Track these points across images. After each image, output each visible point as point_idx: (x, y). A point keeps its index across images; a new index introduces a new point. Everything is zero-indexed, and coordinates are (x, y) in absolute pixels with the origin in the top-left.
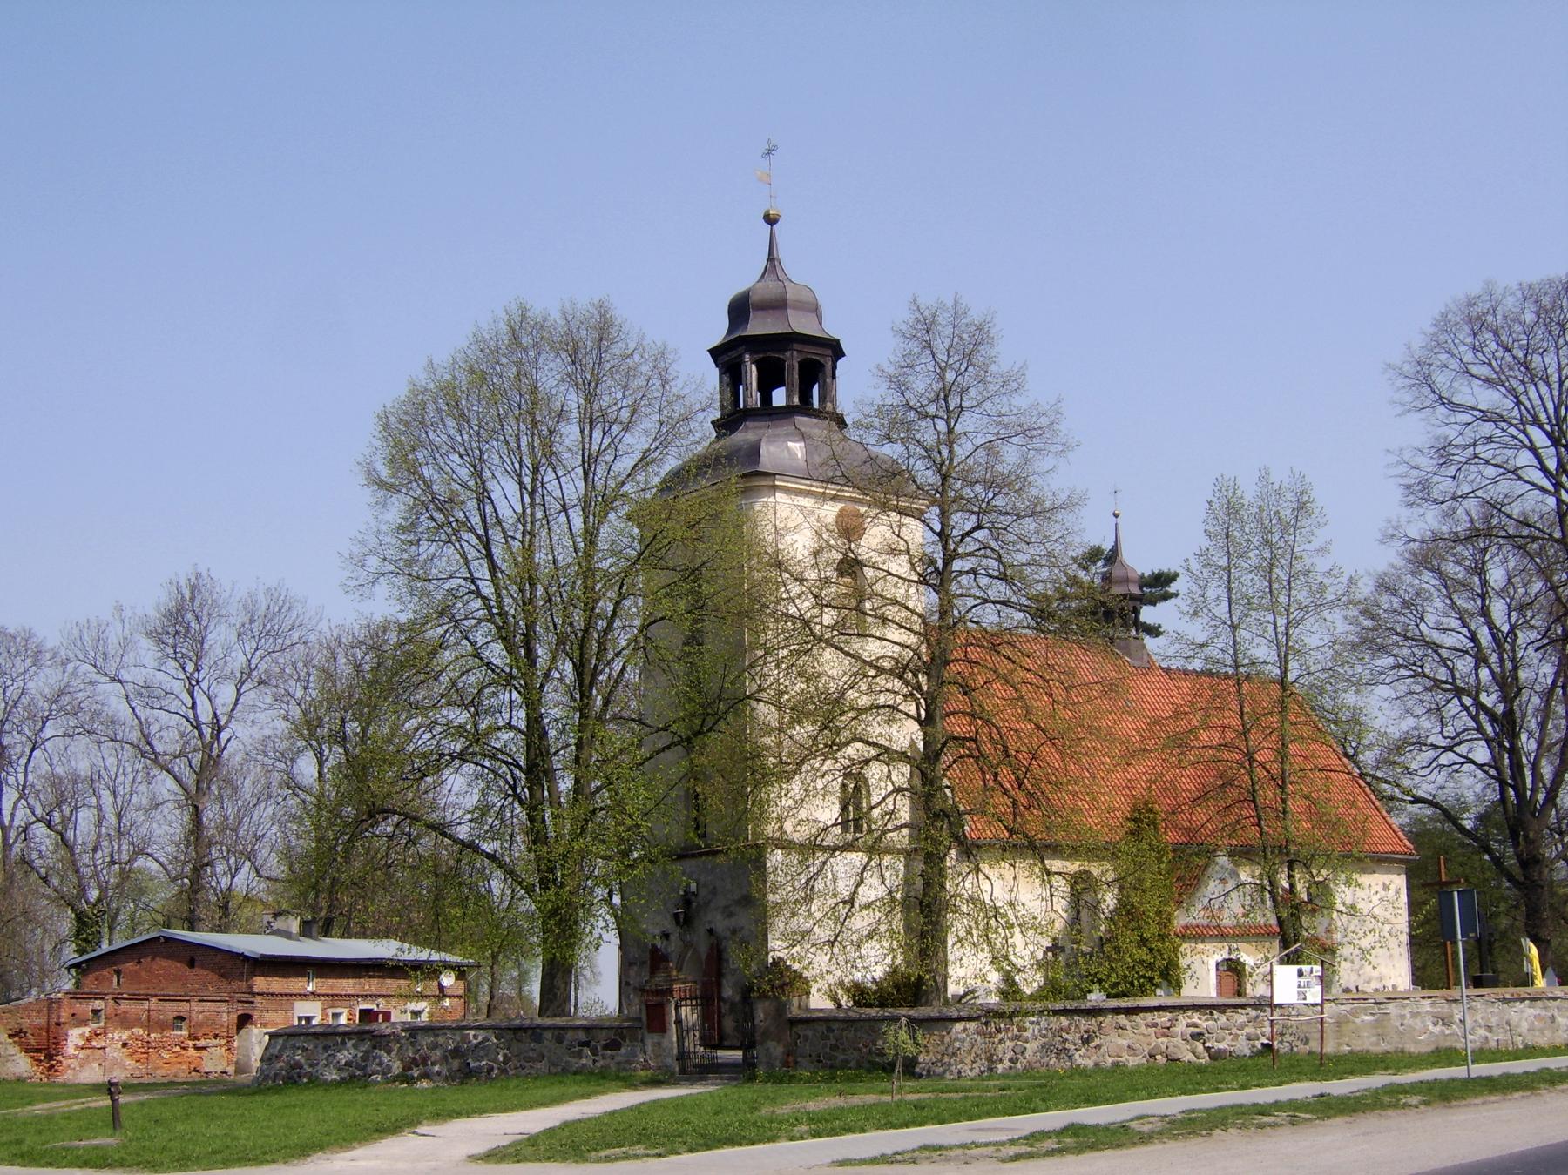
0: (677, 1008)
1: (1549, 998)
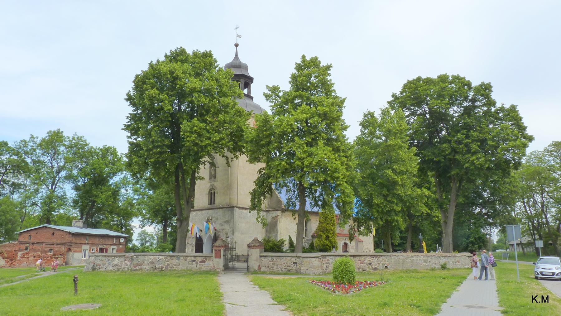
0: (124, 237)
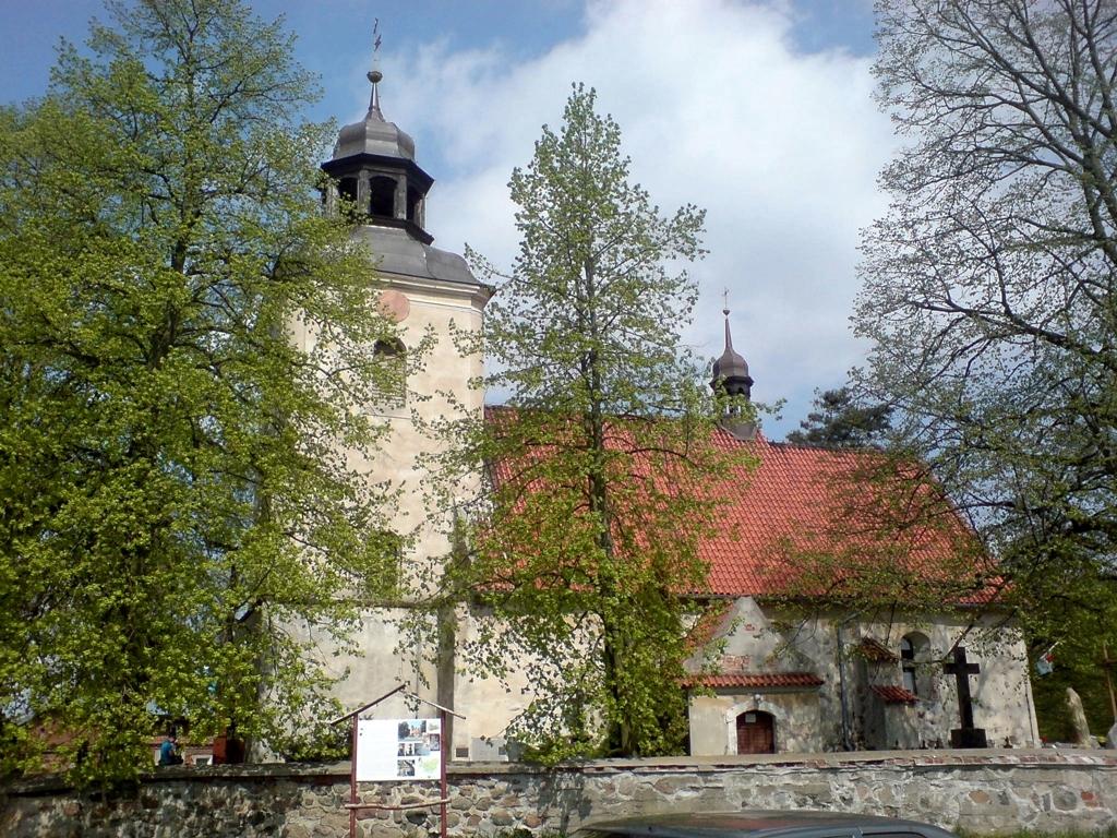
1: (995, 767)
